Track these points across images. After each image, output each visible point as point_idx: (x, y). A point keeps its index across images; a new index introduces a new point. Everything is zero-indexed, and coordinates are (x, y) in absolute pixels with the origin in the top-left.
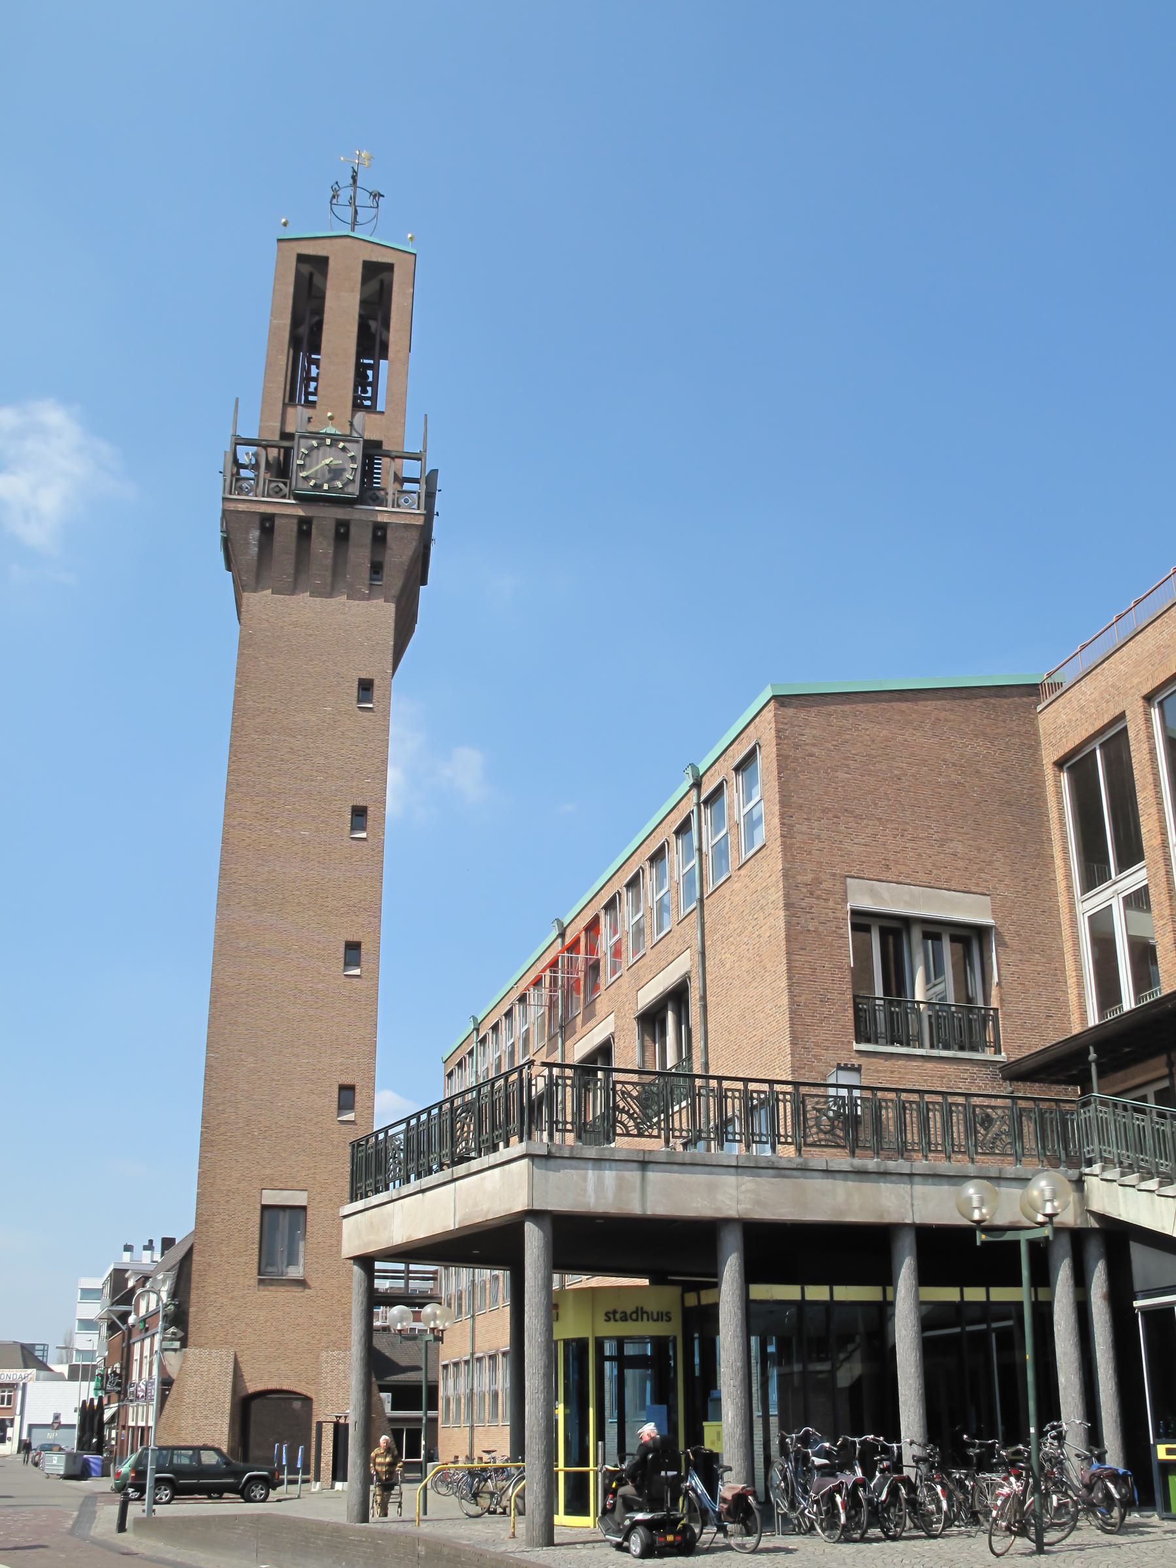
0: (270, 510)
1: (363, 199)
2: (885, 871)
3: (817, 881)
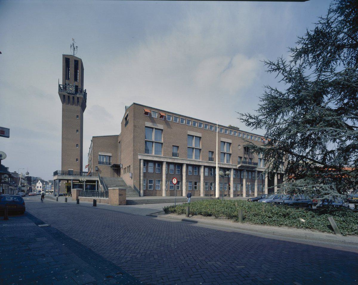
0: (64, 94)
1: (75, 48)
2: (102, 151)
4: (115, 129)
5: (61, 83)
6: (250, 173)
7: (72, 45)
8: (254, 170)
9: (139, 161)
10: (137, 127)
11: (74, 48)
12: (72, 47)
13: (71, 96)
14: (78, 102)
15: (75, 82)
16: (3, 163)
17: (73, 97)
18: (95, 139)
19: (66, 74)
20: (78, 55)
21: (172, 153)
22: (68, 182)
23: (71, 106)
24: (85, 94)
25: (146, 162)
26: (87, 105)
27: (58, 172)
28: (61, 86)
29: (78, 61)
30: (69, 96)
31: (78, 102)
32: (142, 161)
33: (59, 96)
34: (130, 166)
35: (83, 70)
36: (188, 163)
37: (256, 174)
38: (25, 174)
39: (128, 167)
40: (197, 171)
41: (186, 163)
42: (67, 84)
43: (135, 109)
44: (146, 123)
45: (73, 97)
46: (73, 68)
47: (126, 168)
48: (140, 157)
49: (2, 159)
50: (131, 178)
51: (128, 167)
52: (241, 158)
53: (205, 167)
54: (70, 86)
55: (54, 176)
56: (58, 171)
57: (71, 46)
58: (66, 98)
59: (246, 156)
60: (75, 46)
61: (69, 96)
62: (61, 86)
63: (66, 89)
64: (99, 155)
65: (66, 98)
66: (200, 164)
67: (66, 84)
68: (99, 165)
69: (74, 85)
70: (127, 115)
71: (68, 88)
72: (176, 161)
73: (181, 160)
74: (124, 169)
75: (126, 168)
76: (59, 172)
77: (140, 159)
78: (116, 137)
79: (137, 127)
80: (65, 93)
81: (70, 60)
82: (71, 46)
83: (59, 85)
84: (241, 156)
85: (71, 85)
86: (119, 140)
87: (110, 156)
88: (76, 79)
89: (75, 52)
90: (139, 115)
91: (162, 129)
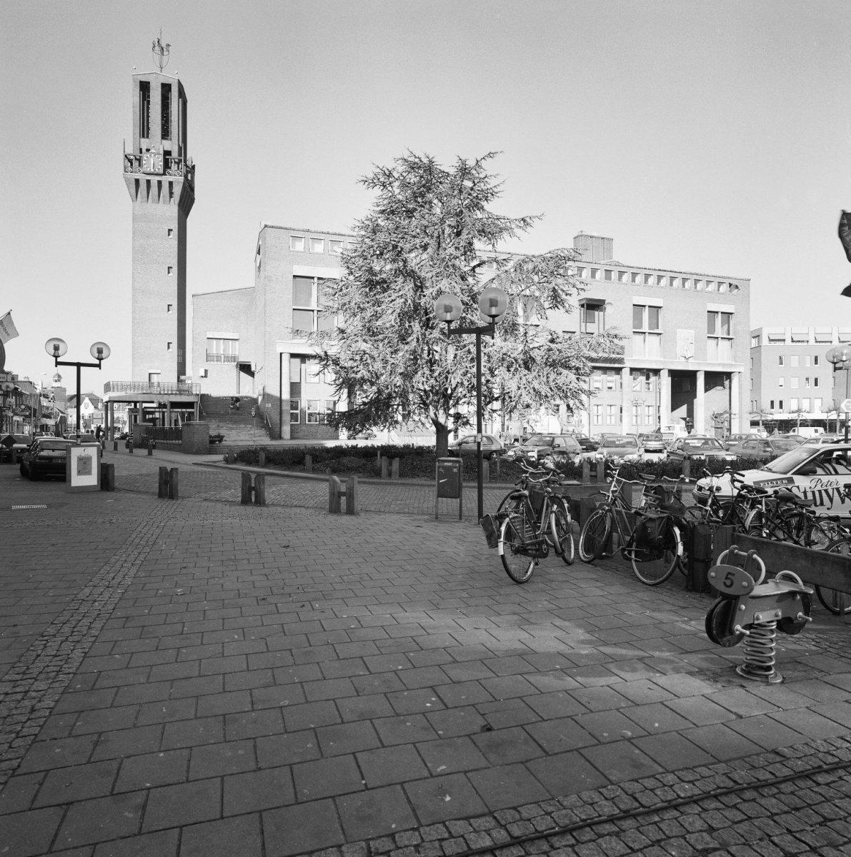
0: (137, 178)
12: (157, 48)
13: (154, 180)
14: (171, 194)
15: (164, 141)
16: (8, 346)
17: (160, 183)
19: (143, 110)
23: (155, 206)
26: (196, 197)
29: (170, 85)
30: (148, 182)
31: (171, 194)
33: (187, 319)
35: (192, 201)
38: (52, 380)
42: (144, 151)
45: (160, 183)
49: (104, 357)
55: (842, 294)
56: (111, 383)
57: (154, 47)
58: (143, 186)
61: (148, 182)
65: (143, 186)
81: (152, 85)
82: (154, 47)
88: (165, 134)
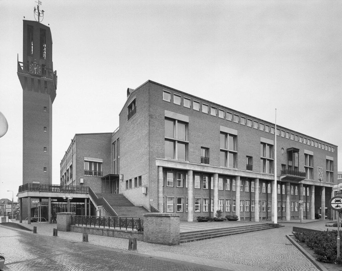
0: (26, 76)
1: (41, 12)
3: (80, 157)
4: (109, 123)
5: (21, 60)
6: (247, 183)
7: (37, 8)
8: (299, 182)
9: (157, 169)
10: (154, 117)
11: (39, 13)
12: (37, 11)
17: (39, 81)
18: (79, 139)
20: (44, 22)
21: (200, 157)
22: (40, 201)
24: (55, 77)
25: (166, 170)
26: (57, 94)
27: (29, 186)
28: (21, 65)
30: (33, 79)
32: (161, 169)
34: (140, 177)
36: (221, 172)
37: (258, 184)
39: (136, 179)
40: (182, 180)
41: (240, 175)
43: (150, 90)
44: (166, 111)
46: (37, 37)
47: (131, 180)
48: (158, 163)
50: (144, 195)
51: (136, 179)
52: (283, 165)
53: (195, 173)
54: (34, 65)
59: (290, 164)
60: (41, 9)
61: (33, 79)
62: (21, 65)
63: (28, 69)
64: (85, 161)
66: (236, 174)
67: (28, 62)
68: (85, 175)
69: (41, 64)
70: (134, 102)
71: (31, 67)
72: (205, 170)
73: (213, 168)
74: (127, 181)
75: (131, 180)
76: (30, 185)
77: (158, 166)
78: (109, 136)
79: (154, 117)
80: (27, 75)
82: (35, 10)
83: (19, 63)
84: (285, 164)
85: (35, 63)
86: (115, 139)
87: (100, 163)
89: (41, 18)
90: (146, 100)
91: (188, 121)
